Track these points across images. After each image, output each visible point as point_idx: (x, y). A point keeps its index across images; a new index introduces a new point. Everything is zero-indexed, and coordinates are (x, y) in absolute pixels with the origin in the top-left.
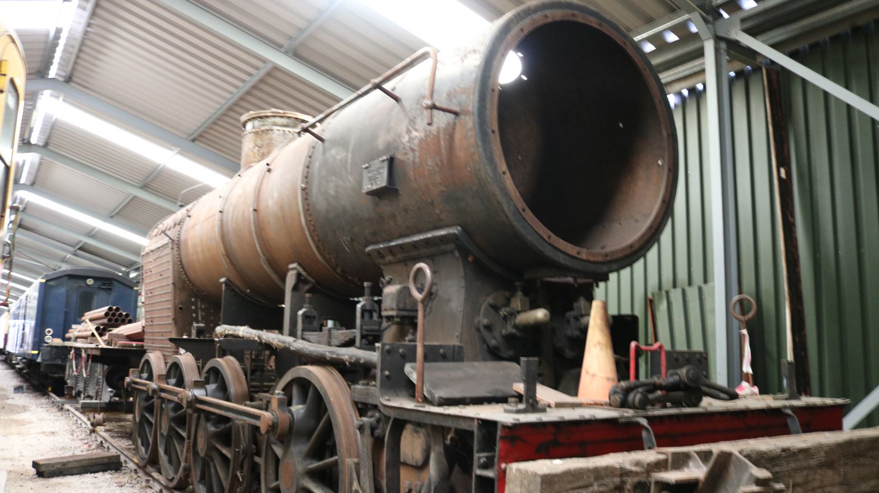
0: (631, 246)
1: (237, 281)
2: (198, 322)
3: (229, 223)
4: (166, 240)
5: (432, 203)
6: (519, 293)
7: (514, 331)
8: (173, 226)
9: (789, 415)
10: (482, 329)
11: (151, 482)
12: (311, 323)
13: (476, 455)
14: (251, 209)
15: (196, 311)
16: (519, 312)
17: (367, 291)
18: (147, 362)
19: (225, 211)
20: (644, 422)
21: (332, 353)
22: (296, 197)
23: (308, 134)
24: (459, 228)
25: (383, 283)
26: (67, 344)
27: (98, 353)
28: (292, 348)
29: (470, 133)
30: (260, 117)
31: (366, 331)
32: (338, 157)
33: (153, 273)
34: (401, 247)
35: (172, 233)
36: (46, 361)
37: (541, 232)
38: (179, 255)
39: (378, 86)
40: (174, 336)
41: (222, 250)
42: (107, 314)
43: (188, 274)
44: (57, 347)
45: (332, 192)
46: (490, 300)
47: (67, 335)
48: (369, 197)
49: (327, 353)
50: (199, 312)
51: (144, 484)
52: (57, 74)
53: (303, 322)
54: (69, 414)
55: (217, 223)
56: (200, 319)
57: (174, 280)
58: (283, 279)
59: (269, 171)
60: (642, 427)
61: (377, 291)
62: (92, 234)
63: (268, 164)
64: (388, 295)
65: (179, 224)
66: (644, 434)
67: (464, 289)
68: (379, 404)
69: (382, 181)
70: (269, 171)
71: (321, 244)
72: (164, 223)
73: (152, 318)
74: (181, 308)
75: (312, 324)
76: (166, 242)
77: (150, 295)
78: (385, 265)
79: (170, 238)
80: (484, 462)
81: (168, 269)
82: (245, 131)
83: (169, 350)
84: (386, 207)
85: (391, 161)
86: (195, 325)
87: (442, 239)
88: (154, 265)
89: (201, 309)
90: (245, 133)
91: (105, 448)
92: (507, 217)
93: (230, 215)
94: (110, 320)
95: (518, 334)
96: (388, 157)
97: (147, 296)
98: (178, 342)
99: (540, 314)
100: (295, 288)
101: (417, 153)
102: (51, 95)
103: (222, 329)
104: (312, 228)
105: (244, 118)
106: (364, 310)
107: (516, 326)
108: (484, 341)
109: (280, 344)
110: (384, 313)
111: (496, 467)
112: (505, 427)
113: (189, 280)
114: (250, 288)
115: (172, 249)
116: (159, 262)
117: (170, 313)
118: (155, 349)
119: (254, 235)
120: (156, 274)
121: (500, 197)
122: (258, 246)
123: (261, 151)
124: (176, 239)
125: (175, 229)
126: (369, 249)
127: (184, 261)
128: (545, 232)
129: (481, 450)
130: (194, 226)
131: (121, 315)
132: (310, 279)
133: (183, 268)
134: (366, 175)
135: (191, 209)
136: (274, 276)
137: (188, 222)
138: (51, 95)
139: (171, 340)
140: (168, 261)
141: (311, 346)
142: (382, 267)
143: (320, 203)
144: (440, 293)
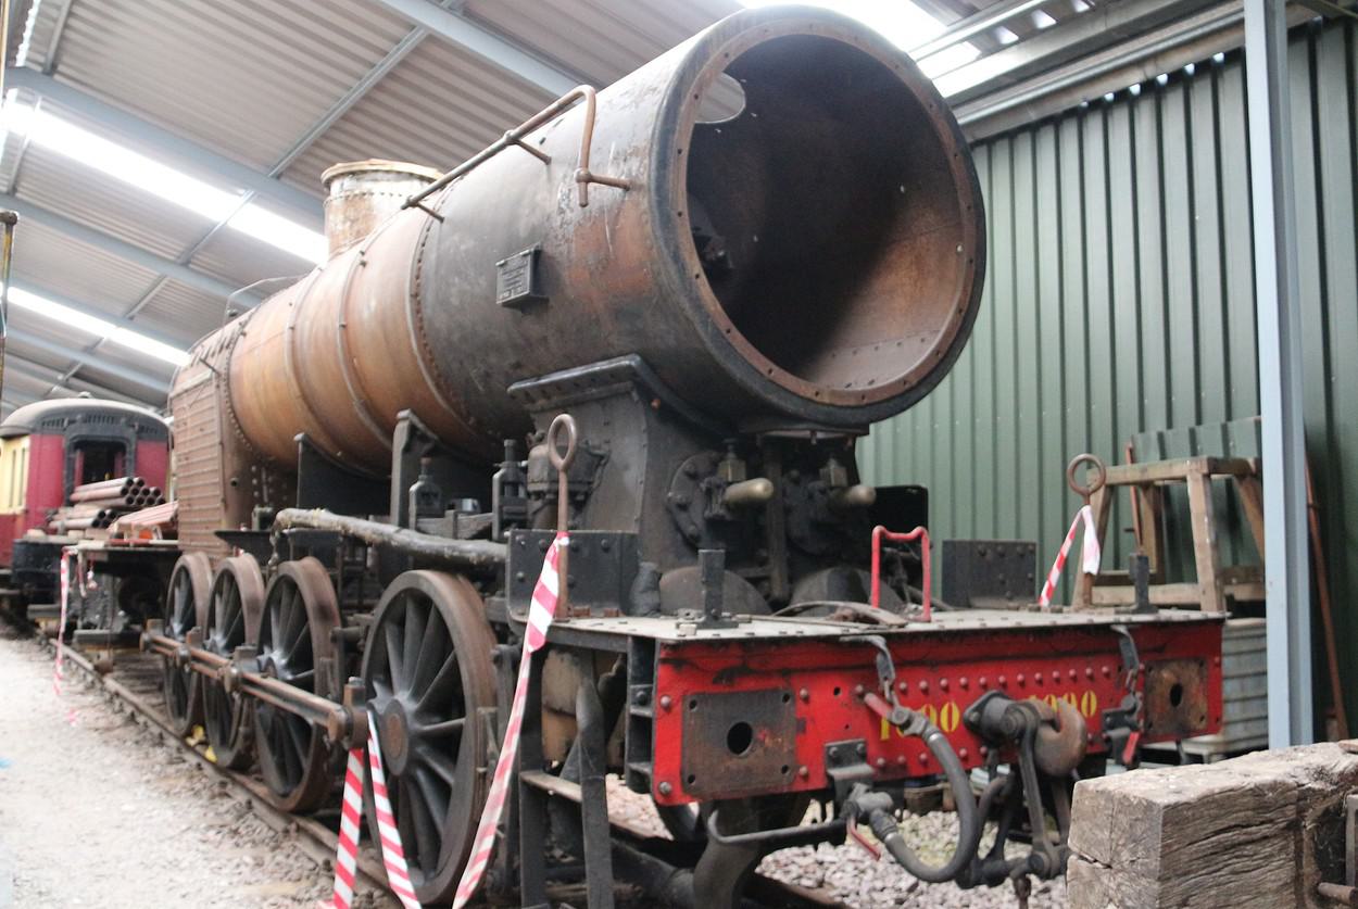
0: (904, 381)
1: (323, 440)
2: (262, 506)
3: (305, 347)
4: (208, 373)
5: (597, 321)
6: (731, 455)
7: (722, 512)
8: (218, 349)
9: (1120, 635)
10: (675, 510)
11: (230, 786)
12: (429, 504)
13: (631, 687)
14: (338, 325)
15: (259, 488)
16: (730, 484)
17: (508, 453)
18: (185, 570)
19: (298, 328)
20: (880, 642)
21: (454, 549)
22: (404, 308)
23: (417, 209)
24: (638, 358)
25: (530, 442)
26: (54, 539)
27: (105, 558)
28: (393, 543)
29: (645, 217)
30: (353, 173)
31: (508, 513)
32: (463, 247)
33: (189, 425)
34: (558, 385)
35: (218, 362)
36: (19, 566)
37: (756, 364)
38: (230, 396)
39: (515, 141)
40: (224, 527)
41: (295, 389)
42: (124, 492)
43: (242, 422)
44: (36, 545)
45: (455, 301)
46: (686, 465)
47: (53, 525)
48: (507, 310)
49: (446, 549)
50: (265, 488)
51: (217, 790)
52: (28, 59)
53: (418, 503)
54: (69, 664)
55: (286, 346)
56: (266, 500)
57: (222, 438)
58: (390, 434)
59: (364, 264)
60: (876, 649)
61: (523, 452)
62: (92, 348)
63: (363, 253)
64: (536, 459)
65: (228, 347)
66: (879, 658)
67: (646, 450)
68: (508, 621)
69: (524, 289)
70: (364, 264)
71: (443, 381)
72: (204, 343)
73: (189, 499)
74: (234, 483)
75: (433, 505)
76: (208, 376)
77: (185, 462)
78: (536, 412)
79: (214, 370)
80: (642, 696)
81: (213, 420)
82: (329, 195)
83: (217, 550)
84: (532, 326)
85: (537, 256)
86: (257, 509)
87: (614, 375)
88: (189, 414)
89: (267, 483)
90: (329, 198)
91: (138, 724)
92: (702, 342)
93: (306, 334)
94: (130, 501)
95: (728, 517)
96: (532, 250)
97: (180, 463)
98: (234, 539)
99: (759, 487)
100: (407, 449)
101: (573, 245)
102: (19, 99)
103: (289, 515)
104: (428, 356)
105: (326, 175)
106: (503, 483)
107: (727, 505)
108: (678, 529)
109: (374, 536)
110: (531, 488)
111: (654, 702)
112: (666, 645)
113: (246, 437)
114: (340, 449)
115: (218, 386)
116: (198, 408)
117: (218, 492)
118: (194, 550)
119: (343, 367)
120: (193, 428)
121: (689, 312)
122: (348, 384)
123: (356, 228)
124: (223, 371)
125: (221, 355)
126: (513, 387)
127: (238, 407)
128: (762, 364)
129: (636, 680)
130: (251, 351)
131: (146, 492)
132: (430, 434)
133: (235, 417)
134: (501, 280)
135: (246, 322)
136: (375, 430)
137: (242, 345)
138: (19, 99)
139: (219, 534)
140: (212, 408)
141: (422, 539)
142: (533, 416)
143: (439, 320)
144: (614, 457)
